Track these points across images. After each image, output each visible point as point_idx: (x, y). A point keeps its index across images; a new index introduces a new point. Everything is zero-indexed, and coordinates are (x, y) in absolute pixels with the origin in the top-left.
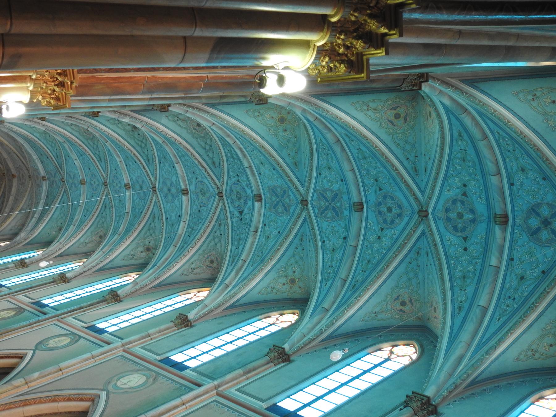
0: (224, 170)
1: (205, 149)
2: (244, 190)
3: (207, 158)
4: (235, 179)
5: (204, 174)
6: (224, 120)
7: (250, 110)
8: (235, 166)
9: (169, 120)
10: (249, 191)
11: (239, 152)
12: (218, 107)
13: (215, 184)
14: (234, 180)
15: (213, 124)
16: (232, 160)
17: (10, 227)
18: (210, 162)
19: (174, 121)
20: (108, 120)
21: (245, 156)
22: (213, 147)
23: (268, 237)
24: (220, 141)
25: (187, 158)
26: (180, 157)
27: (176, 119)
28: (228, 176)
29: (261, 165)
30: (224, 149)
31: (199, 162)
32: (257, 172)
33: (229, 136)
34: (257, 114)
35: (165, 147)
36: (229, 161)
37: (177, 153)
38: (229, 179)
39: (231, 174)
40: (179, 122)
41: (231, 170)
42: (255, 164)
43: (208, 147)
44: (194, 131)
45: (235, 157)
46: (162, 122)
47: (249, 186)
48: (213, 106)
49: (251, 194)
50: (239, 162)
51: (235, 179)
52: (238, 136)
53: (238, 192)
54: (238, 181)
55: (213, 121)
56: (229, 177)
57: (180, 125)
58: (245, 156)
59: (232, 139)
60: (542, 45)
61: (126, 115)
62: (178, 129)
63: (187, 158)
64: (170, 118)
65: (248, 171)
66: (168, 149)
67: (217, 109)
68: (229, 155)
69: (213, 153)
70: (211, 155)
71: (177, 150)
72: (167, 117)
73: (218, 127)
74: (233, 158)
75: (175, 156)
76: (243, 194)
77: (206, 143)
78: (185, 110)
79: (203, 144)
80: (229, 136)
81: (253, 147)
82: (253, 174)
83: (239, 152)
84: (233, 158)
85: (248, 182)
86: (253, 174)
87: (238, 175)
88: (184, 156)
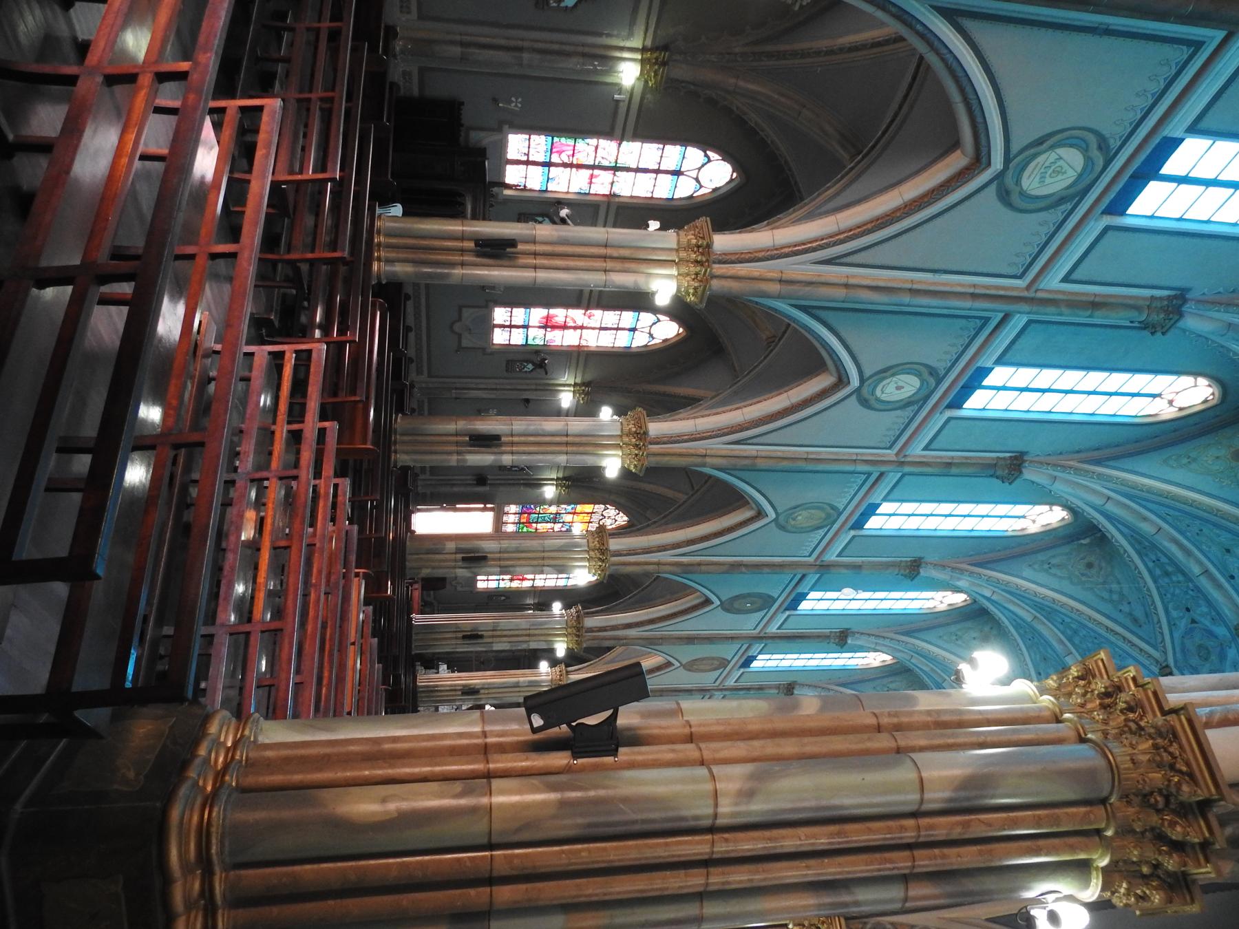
0: (1157, 615)
1: (1111, 601)
2: (1211, 634)
3: (1121, 618)
4: (1184, 621)
5: (1121, 649)
6: (1124, 483)
7: (1170, 457)
8: (1177, 591)
9: (1034, 569)
10: (1221, 631)
11: (1174, 549)
12: (1107, 463)
13: (1150, 656)
14: (1183, 624)
15: (1109, 498)
16: (1166, 580)
18: (1128, 622)
19: (1046, 571)
20: (940, 637)
21: (1188, 553)
22: (1124, 593)
23: (1228, 551)
24: (1130, 543)
25: (1083, 632)
26: (1070, 640)
27: (1046, 566)
28: (1169, 622)
29: (1227, 557)
30: (1143, 561)
31: (1107, 628)
32: (1221, 573)
33: (1145, 519)
34: (1185, 461)
35: (1040, 627)
36: (1162, 586)
37: (1063, 633)
38: (1173, 628)
39: (1174, 614)
40: (1053, 571)
41: (1170, 606)
42: (1215, 562)
43: (1115, 597)
44: (1084, 579)
45: (1170, 569)
46: (1025, 574)
47: (1218, 617)
48: (1098, 462)
49: (1228, 634)
50: (1181, 578)
51: (1184, 621)
52: (1162, 510)
53: (1200, 646)
54: (1193, 621)
55: (1106, 491)
56: (1172, 625)
57: (1055, 575)
58: (1188, 553)
59: (1152, 522)
60: (355, 548)
61: (962, 571)
62: (1055, 583)
63: (1084, 632)
64: (1036, 566)
65: (1204, 582)
66: (1048, 631)
67: (1107, 467)
68: (1158, 572)
69: (1129, 603)
70: (1126, 608)
71: (1061, 627)
72: (1030, 566)
73: (1119, 503)
74: (1167, 574)
75: (1061, 642)
76: (1211, 643)
77: (1111, 591)
78: (1051, 475)
79: (1106, 595)
80: (1145, 519)
81: (1198, 522)
82: (1219, 586)
83: (1174, 549)
84: (1167, 574)
85: (1214, 613)
86: (1219, 586)
87: (1188, 610)
88: (1076, 632)
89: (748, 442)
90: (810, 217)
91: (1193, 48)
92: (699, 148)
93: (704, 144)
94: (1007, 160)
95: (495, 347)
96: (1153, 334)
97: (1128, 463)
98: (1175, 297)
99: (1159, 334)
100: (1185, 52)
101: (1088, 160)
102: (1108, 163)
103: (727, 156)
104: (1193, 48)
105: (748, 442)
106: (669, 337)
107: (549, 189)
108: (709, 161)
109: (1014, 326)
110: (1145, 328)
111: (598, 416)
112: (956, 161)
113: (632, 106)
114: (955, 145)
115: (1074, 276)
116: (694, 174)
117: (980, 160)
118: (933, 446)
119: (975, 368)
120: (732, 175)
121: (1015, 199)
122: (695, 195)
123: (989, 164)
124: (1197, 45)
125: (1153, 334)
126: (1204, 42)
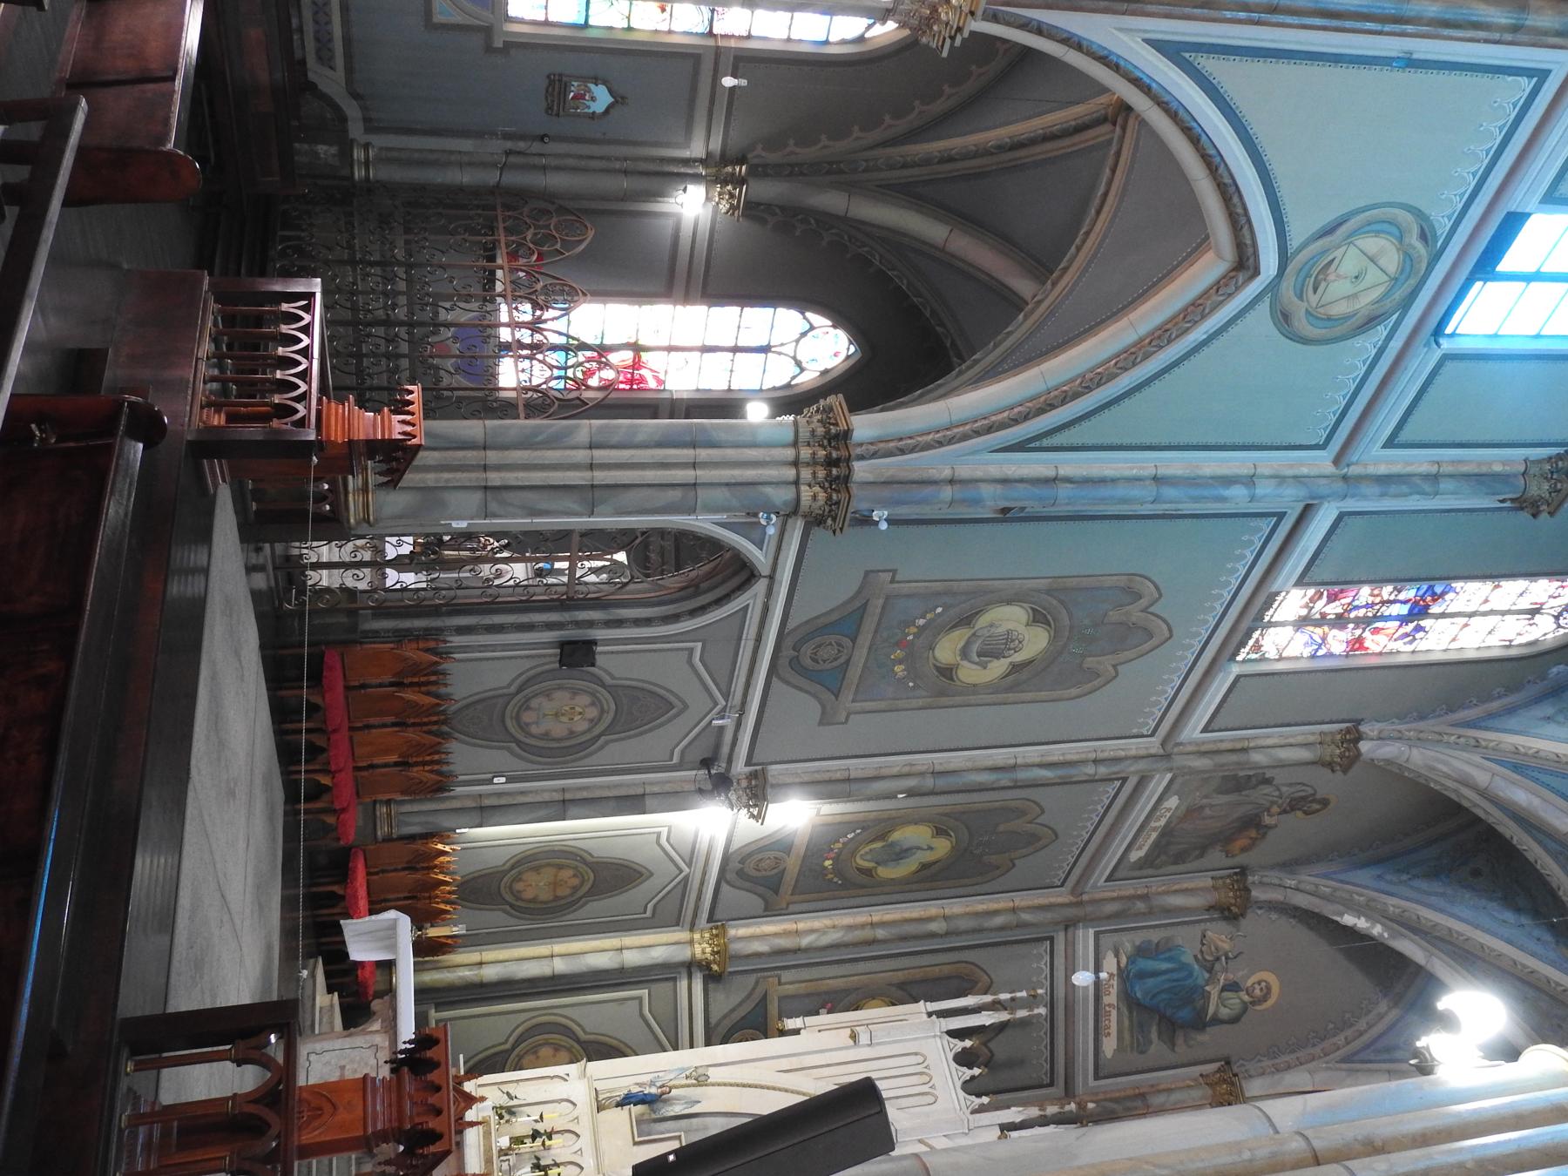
9: (1558, 723)
89: (1046, 442)
90: (993, 373)
91: (1535, 79)
92: (789, 306)
93: (802, 299)
94: (1284, 259)
95: (503, 394)
96: (1535, 516)
97: (1512, 722)
98: (1348, 731)
99: (1544, 516)
100: (1526, 84)
101: (1408, 257)
102: (1436, 257)
103: (841, 318)
104: (1535, 79)
105: (1046, 442)
106: (829, 367)
107: (591, 22)
108: (812, 328)
109: (1302, 554)
110: (1293, 809)
111: (743, 417)
112: (1207, 269)
113: (705, 119)
114: (1202, 242)
115: (1404, 436)
116: (789, 350)
117: (1245, 263)
118: (1214, 726)
119: (1266, 594)
120: (848, 349)
121: (1302, 324)
122: (793, 383)
123: (1256, 272)
124: (1542, 75)
125: (1535, 516)
126: (1549, 71)
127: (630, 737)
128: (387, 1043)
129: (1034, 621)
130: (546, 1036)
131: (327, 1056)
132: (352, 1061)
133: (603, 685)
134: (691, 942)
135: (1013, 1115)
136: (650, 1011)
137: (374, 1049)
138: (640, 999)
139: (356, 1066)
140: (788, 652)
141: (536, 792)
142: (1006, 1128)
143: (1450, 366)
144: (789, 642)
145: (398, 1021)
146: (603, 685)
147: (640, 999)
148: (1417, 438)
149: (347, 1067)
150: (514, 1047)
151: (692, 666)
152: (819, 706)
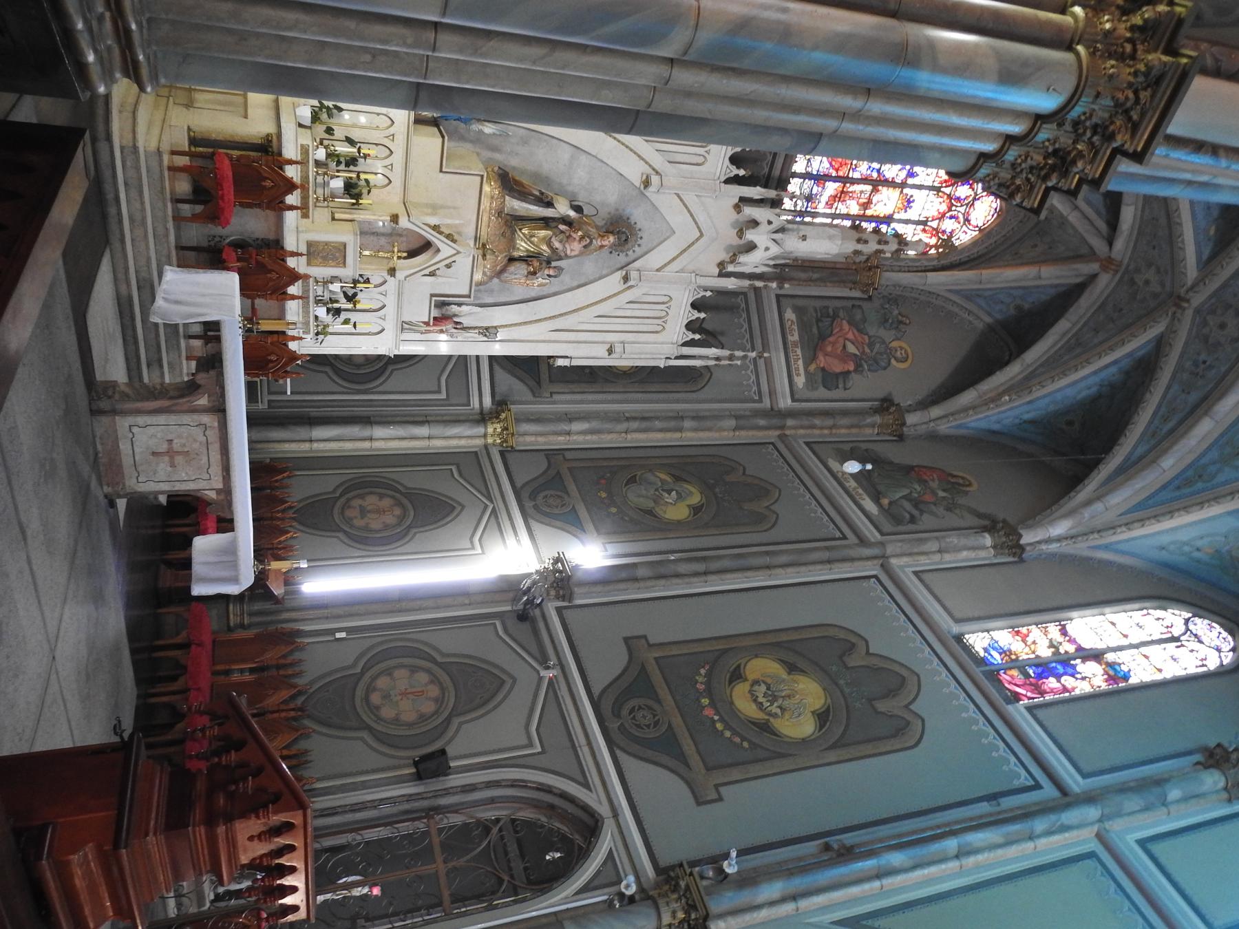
17: (1165, 540)
115: (925, 576)
127: (455, 655)
128: (216, 424)
129: (818, 715)
130: (412, 732)
131: (151, 430)
132: (180, 437)
133: (401, 493)
134: (485, 436)
135: (756, 192)
136: (537, 730)
137: (202, 428)
138: (439, 392)
139: (183, 441)
140: (614, 725)
141: (374, 804)
142: (744, 200)
143: (1087, 768)
144: (607, 707)
145: (229, 426)
146: (401, 493)
147: (439, 392)
148: (1163, 860)
149: (175, 441)
150: (363, 673)
151: (439, 380)
152: (627, 658)
